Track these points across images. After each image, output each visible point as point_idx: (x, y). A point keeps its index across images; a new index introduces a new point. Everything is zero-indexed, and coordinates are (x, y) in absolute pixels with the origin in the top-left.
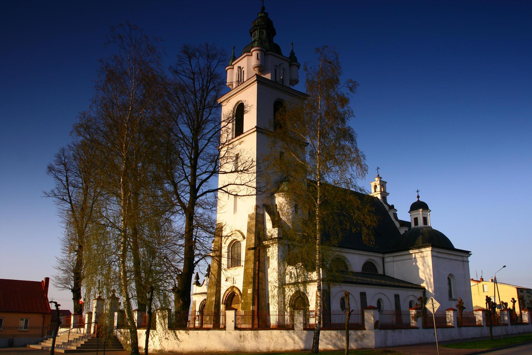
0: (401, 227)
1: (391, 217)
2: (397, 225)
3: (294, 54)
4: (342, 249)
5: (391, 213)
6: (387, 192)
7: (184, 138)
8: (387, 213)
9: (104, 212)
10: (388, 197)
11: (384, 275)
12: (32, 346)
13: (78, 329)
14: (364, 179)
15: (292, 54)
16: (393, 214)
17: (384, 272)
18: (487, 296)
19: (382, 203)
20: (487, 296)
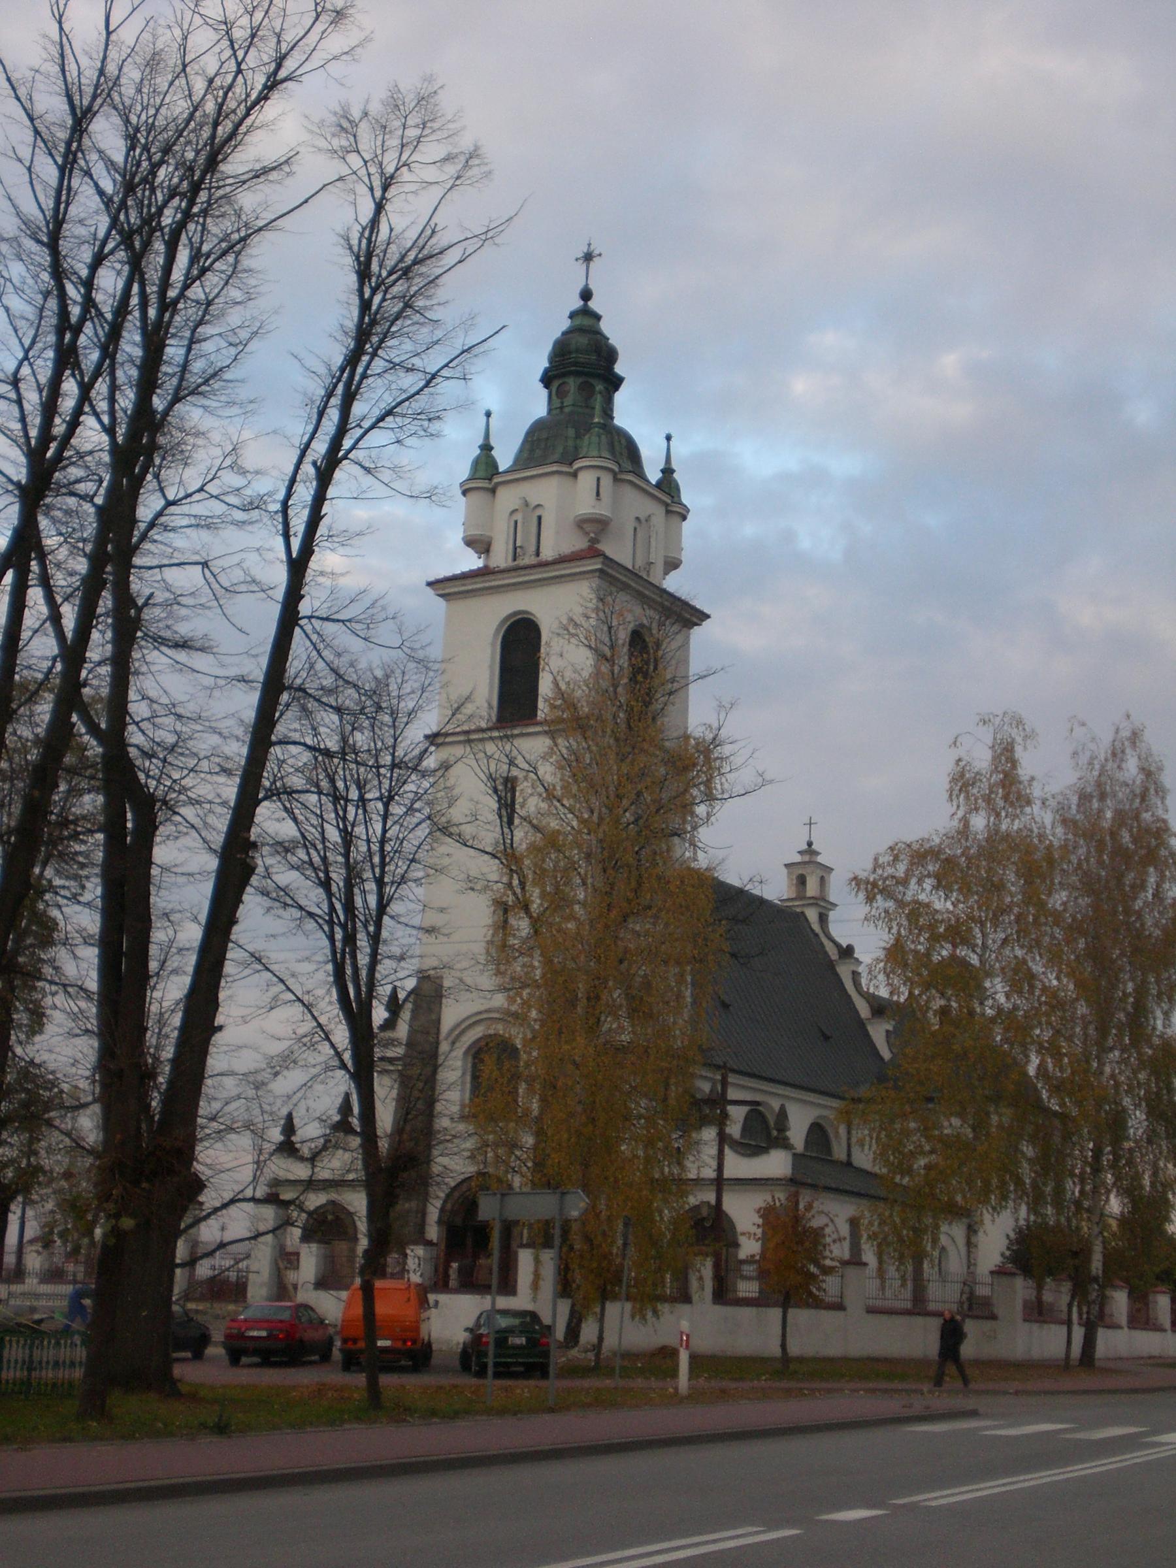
0: (873, 1015)
1: (879, 1047)
2: (864, 1010)
3: (672, 471)
4: (476, 583)
5: (844, 971)
6: (832, 899)
7: (97, 374)
8: (831, 966)
9: (345, 1150)
10: (832, 915)
11: (849, 1163)
12: (49, 454)
13: (132, 571)
14: (338, 109)
15: (668, 471)
16: (850, 976)
17: (849, 1155)
18: (708, 617)
19: (817, 935)
20: (708, 617)
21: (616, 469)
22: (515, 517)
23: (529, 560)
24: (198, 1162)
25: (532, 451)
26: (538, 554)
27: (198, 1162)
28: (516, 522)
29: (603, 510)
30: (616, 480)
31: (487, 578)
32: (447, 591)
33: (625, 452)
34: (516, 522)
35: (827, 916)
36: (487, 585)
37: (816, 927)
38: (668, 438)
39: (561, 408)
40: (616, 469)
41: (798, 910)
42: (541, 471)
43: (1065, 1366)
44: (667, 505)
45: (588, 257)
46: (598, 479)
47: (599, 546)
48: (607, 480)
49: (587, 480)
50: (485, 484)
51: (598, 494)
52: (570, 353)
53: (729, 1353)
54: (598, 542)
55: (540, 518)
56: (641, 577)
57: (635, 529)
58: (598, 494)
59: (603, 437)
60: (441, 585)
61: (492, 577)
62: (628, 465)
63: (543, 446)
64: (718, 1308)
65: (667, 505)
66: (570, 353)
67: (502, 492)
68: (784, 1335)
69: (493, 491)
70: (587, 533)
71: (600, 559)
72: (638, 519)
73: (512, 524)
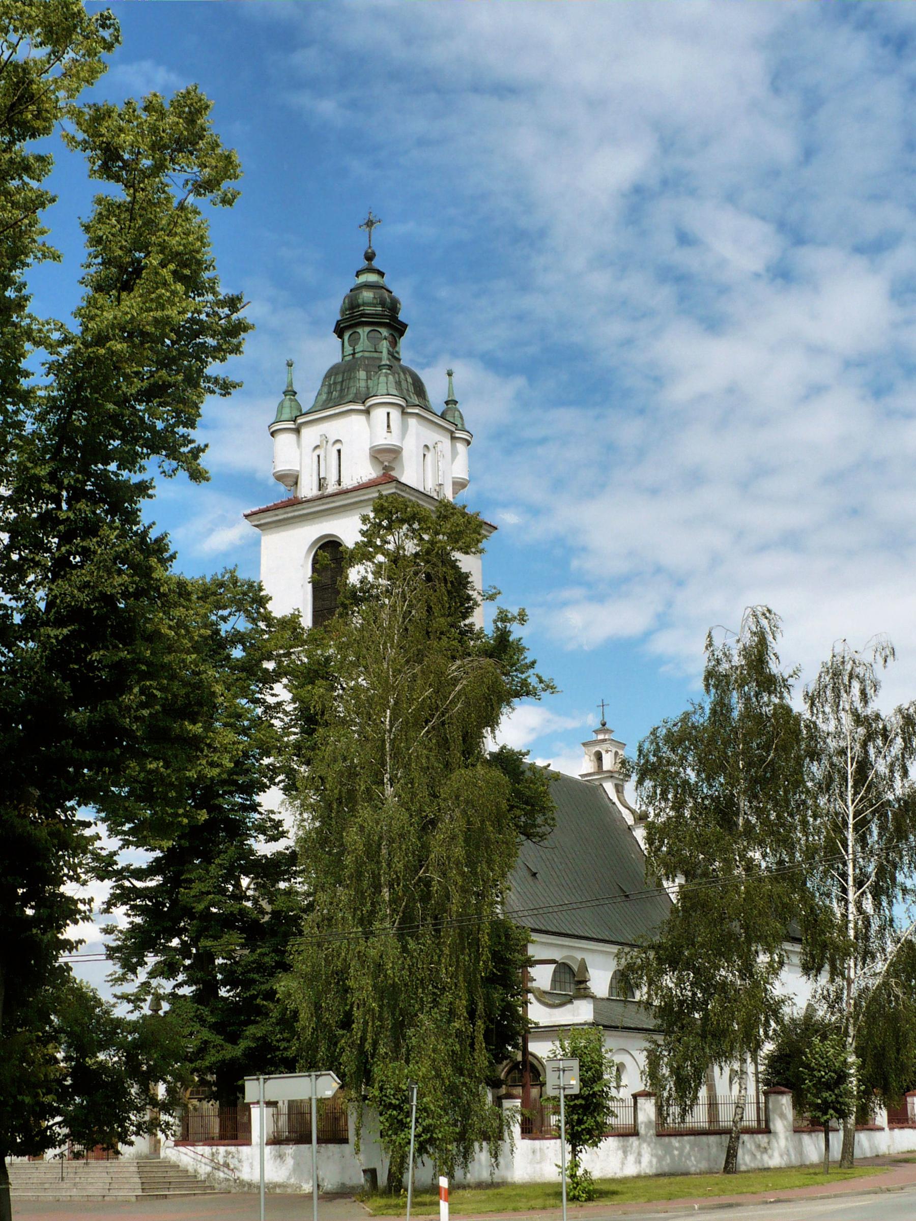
19: (614, 803)
21: (403, 403)
22: (317, 452)
23: (332, 488)
24: (493, 731)
25: (330, 393)
26: (339, 483)
27: (493, 731)
28: (319, 456)
29: (392, 440)
30: (404, 413)
31: (295, 508)
32: (262, 522)
33: (411, 389)
34: (319, 456)
35: (622, 786)
36: (296, 513)
37: (615, 799)
38: (450, 374)
39: (354, 354)
40: (403, 403)
41: (597, 783)
42: (337, 411)
43: (826, 1166)
44: (452, 432)
45: (370, 224)
46: (388, 414)
47: (393, 473)
48: (395, 414)
49: (379, 414)
50: (291, 425)
51: (388, 426)
52: (359, 306)
53: (539, 1181)
54: (393, 469)
55: (339, 451)
56: (432, 498)
57: (424, 455)
58: (388, 426)
59: (391, 377)
60: (255, 517)
61: (300, 507)
62: (415, 400)
63: (338, 388)
64: (527, 1142)
65: (452, 432)
66: (359, 306)
67: (305, 431)
68: (301, 459)
69: (297, 431)
70: (382, 463)
71: (394, 484)
72: (426, 446)
73: (316, 459)
